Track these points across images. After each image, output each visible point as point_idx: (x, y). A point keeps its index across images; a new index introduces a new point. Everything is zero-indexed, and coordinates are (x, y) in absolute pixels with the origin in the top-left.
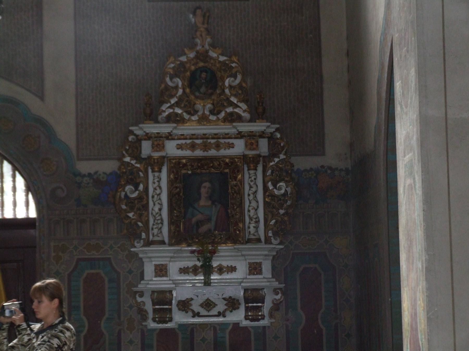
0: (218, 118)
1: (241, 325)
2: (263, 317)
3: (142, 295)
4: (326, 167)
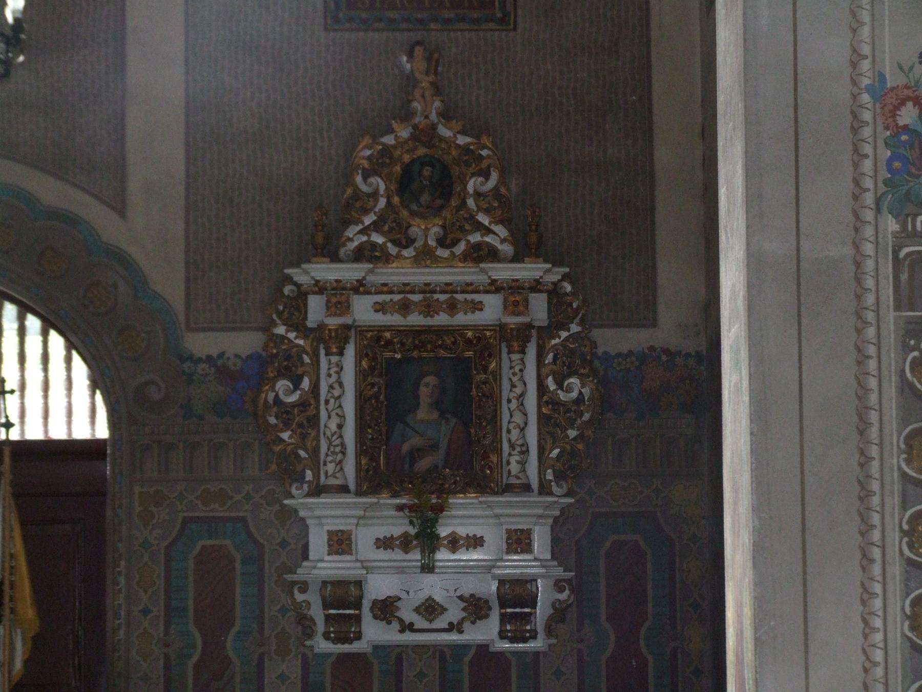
0: (452, 253)
1: (492, 649)
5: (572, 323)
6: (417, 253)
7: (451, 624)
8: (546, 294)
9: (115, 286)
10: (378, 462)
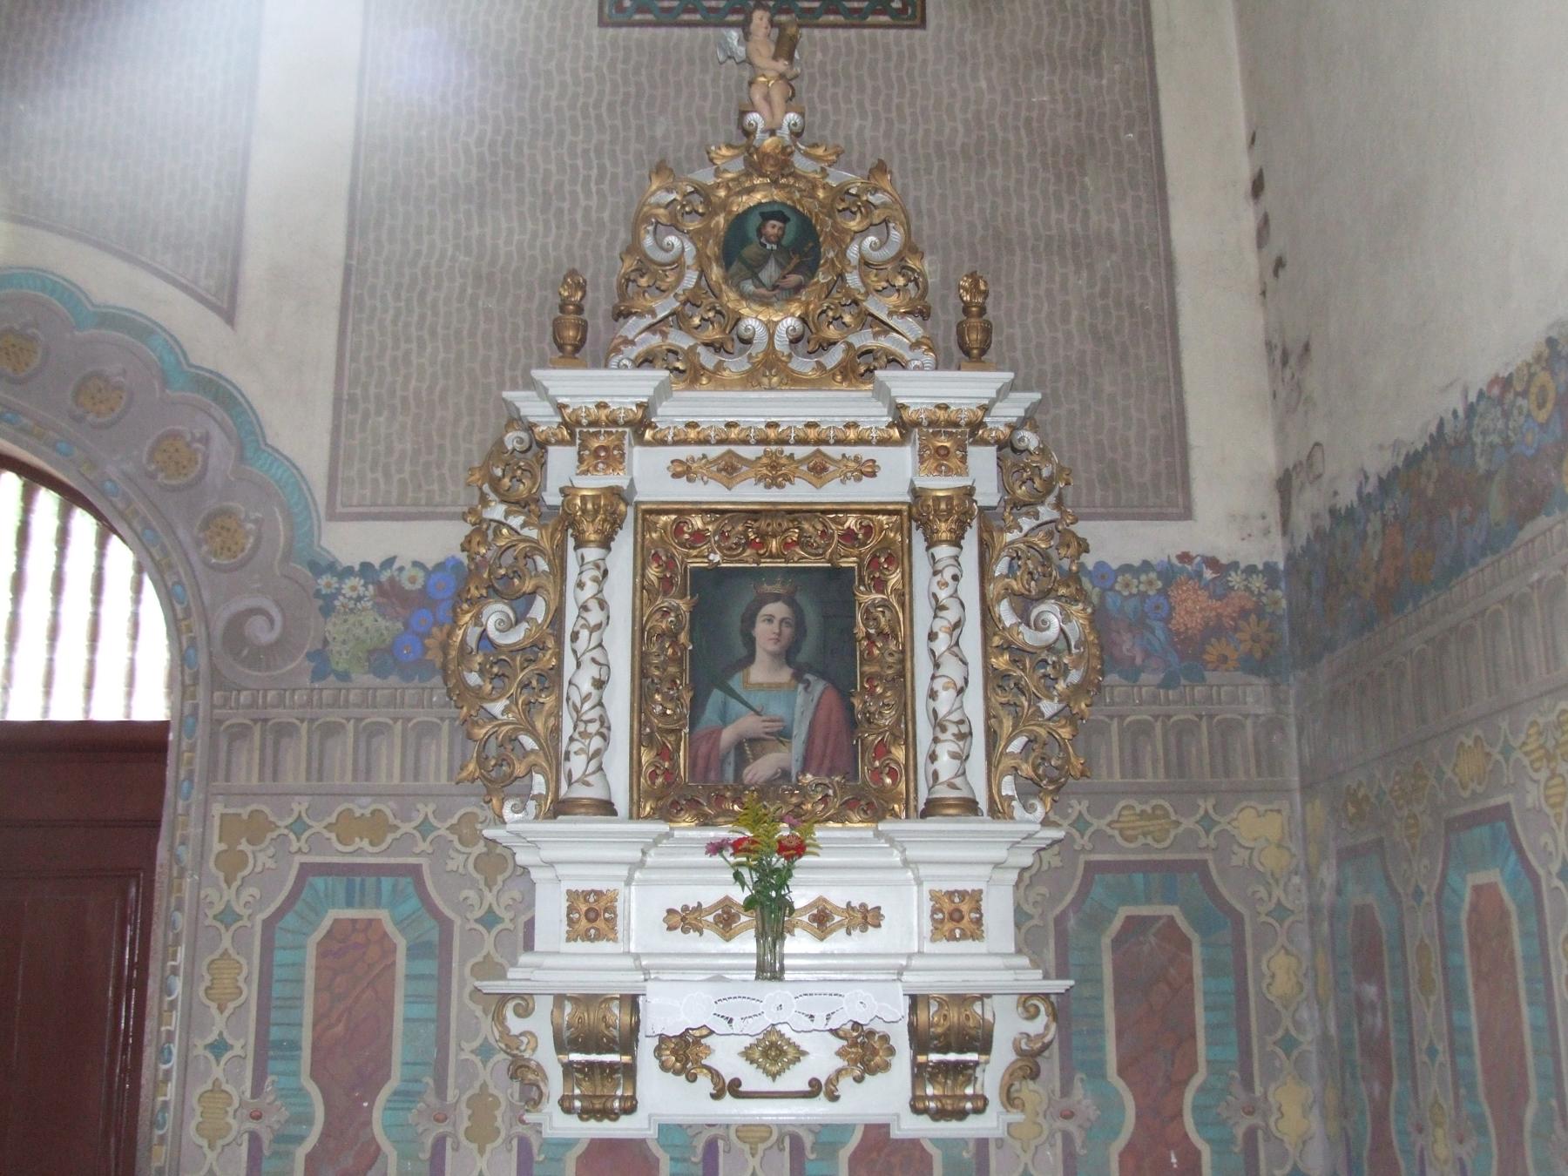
0: (820, 366)
1: (895, 1133)
2: (980, 1104)
3: (524, 1011)
4: (1198, 559)
5: (1042, 503)
6: (753, 364)
7: (814, 1083)
8: (994, 448)
9: (206, 439)
10: (675, 765)
